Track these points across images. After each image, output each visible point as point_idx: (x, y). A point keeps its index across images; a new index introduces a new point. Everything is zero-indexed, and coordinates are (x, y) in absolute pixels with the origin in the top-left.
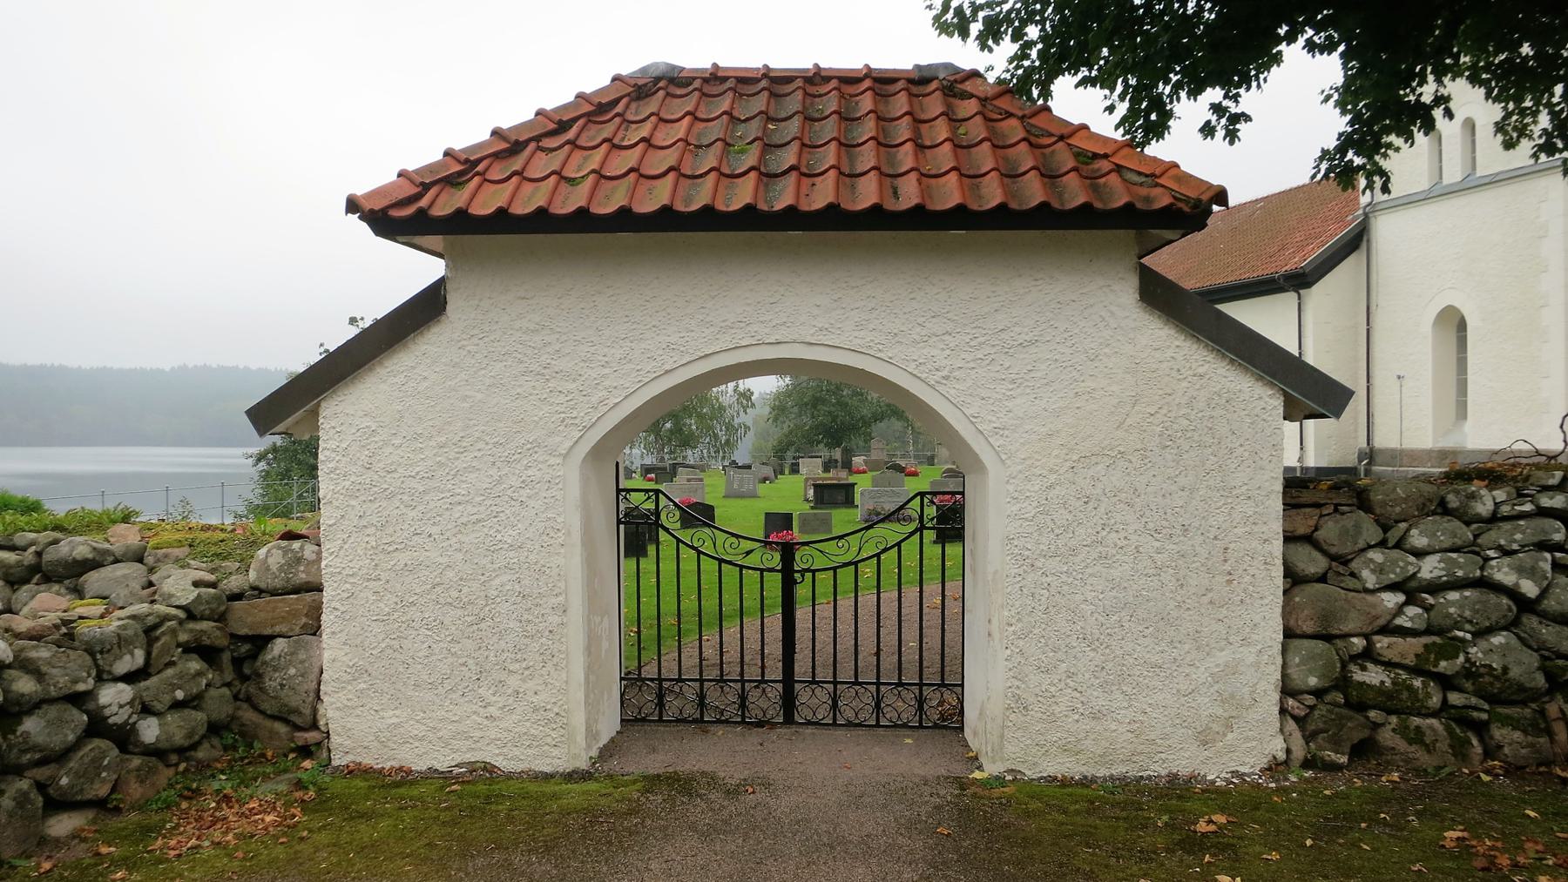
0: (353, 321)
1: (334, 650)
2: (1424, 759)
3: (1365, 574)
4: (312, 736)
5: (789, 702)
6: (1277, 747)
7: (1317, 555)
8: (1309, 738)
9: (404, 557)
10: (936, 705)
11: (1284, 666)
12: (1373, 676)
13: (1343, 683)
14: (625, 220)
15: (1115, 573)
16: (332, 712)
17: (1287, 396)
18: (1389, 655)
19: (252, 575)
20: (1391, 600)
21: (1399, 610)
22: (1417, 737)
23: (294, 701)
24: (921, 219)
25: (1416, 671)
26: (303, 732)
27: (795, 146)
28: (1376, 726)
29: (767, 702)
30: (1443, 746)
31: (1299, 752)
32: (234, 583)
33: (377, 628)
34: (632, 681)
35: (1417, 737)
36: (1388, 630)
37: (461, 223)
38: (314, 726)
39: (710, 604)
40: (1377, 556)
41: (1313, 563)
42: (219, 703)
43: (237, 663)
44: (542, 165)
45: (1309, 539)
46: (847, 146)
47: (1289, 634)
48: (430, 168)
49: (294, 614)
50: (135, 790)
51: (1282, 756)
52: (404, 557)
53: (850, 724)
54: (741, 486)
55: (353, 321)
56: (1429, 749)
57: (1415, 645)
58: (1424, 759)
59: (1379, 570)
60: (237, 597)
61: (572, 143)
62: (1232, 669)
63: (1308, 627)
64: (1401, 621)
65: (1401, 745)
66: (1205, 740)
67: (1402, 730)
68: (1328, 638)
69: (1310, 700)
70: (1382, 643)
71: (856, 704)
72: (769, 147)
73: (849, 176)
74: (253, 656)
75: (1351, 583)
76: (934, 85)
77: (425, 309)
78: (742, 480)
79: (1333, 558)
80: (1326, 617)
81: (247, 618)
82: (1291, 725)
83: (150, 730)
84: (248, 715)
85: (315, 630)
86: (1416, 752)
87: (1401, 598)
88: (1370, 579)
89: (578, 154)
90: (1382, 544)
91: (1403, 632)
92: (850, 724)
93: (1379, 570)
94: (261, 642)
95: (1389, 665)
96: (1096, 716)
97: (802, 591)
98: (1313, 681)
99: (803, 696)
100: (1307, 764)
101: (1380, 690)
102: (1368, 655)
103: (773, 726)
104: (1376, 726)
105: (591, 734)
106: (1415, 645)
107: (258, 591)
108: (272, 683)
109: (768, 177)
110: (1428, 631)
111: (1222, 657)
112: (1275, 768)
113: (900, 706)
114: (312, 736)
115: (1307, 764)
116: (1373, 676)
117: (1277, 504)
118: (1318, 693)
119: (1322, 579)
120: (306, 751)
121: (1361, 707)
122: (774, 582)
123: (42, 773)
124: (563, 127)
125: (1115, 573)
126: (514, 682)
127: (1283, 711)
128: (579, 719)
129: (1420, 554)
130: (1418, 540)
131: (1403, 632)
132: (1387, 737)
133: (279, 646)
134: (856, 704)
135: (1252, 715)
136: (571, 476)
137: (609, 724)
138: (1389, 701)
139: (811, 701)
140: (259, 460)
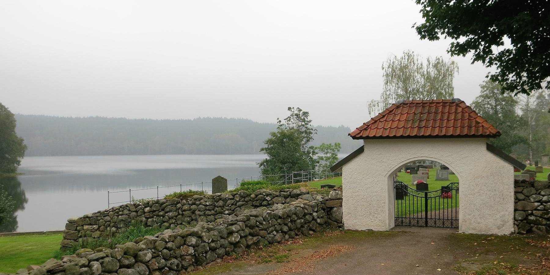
0: (289, 109)
1: (345, 209)
2: (541, 233)
3: (531, 199)
4: (341, 224)
5: (426, 222)
6: (512, 230)
7: (523, 196)
8: (519, 229)
9: (357, 194)
10: (454, 223)
11: (515, 215)
12: (532, 218)
13: (526, 218)
14: (395, 137)
15: (482, 198)
16: (344, 220)
17: (514, 168)
18: (535, 214)
19: (329, 197)
20: (536, 204)
21: (539, 206)
22: (539, 229)
23: (338, 218)
24: (445, 137)
25: (541, 217)
26: (339, 224)
27: (425, 121)
28: (532, 227)
29: (422, 222)
30: (544, 231)
31: (517, 231)
32: (327, 198)
33: (352, 206)
34: (397, 219)
35: (539, 229)
36: (536, 209)
37: (367, 138)
38: (341, 223)
39: (415, 209)
40: (534, 196)
41: (521, 196)
42: (325, 219)
43: (327, 212)
44: (381, 125)
45: (521, 192)
46: (435, 120)
47: (516, 210)
48: (361, 127)
49: (337, 203)
50: (318, 229)
51: (513, 232)
52: (357, 194)
53: (438, 227)
54: (442, 176)
55: (289, 109)
56: (542, 231)
57: (541, 212)
58: (541, 233)
59: (534, 198)
60: (327, 200)
61: (385, 120)
62: (504, 216)
63: (520, 209)
64: (539, 208)
65: (536, 230)
66: (499, 228)
67: (537, 228)
68: (525, 211)
69: (519, 222)
70: (534, 212)
71: (439, 223)
72: (421, 121)
73: (433, 128)
74: (330, 211)
75: (529, 201)
76: (455, 104)
77: (360, 151)
78: (442, 174)
79: (527, 196)
80: (524, 207)
81: (329, 204)
82: (516, 226)
83: (319, 221)
84: (330, 221)
85: (341, 206)
86: (539, 231)
87: (539, 204)
88: (532, 200)
89: (387, 122)
90: (536, 194)
91: (539, 210)
92: (438, 227)
93: (534, 198)
94: (332, 208)
95: (536, 216)
96: (479, 223)
97: (429, 201)
98: (520, 218)
99: (429, 221)
100: (518, 233)
101: (533, 220)
102: (532, 214)
103: (423, 227)
104: (532, 227)
105: (389, 225)
106: (541, 212)
107: (331, 199)
108: (334, 215)
109: (419, 128)
110: (544, 210)
111: (502, 213)
112: (512, 233)
113: (448, 224)
114: (341, 224)
115: (518, 233)
116: (532, 218)
117: (512, 186)
118: (521, 221)
119: (524, 200)
120: (340, 227)
121: (530, 224)
122: (424, 199)
123: (309, 224)
124: (384, 116)
125: (482, 198)
126: (376, 215)
127: (514, 224)
128: (387, 222)
129: (543, 196)
130: (543, 193)
131: (539, 210)
132: (534, 229)
133: (335, 209)
134: (439, 223)
135: (508, 224)
136: (386, 180)
137: (393, 225)
138: (536, 223)
139: (430, 223)
140: (261, 165)
